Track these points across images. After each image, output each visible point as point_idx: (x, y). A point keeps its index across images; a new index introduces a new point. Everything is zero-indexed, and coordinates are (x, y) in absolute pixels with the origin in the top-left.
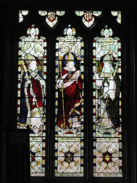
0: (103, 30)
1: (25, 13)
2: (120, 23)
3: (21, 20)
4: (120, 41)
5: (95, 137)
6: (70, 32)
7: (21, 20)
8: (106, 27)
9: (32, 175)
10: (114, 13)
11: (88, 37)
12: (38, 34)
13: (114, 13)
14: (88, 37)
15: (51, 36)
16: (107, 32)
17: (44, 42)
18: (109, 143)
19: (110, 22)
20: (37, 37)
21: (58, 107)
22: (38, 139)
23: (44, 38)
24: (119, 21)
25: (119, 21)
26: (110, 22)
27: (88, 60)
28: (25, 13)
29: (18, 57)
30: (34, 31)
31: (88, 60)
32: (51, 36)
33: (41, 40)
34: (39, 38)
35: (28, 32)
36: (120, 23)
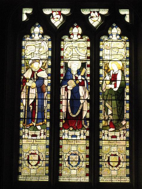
0: (71, 28)
1: (29, 11)
2: (129, 22)
3: (25, 18)
4: (51, 40)
5: (127, 141)
6: (76, 30)
7: (25, 18)
8: (75, 25)
9: (101, 181)
10: (123, 12)
11: (95, 36)
12: (119, 34)
13: (123, 12)
14: (95, 36)
15: (56, 36)
16: (115, 31)
17: (48, 41)
18: (116, 145)
19: (119, 21)
20: (79, 37)
21: (26, 111)
22: (120, 143)
23: (49, 38)
24: (127, 19)
25: (127, 19)
26: (119, 21)
27: (95, 59)
28: (29, 11)
29: (20, 57)
30: (37, 30)
31: (95, 59)
32: (56, 36)
33: (84, 39)
34: (82, 38)
35: (109, 32)
36: (129, 22)
